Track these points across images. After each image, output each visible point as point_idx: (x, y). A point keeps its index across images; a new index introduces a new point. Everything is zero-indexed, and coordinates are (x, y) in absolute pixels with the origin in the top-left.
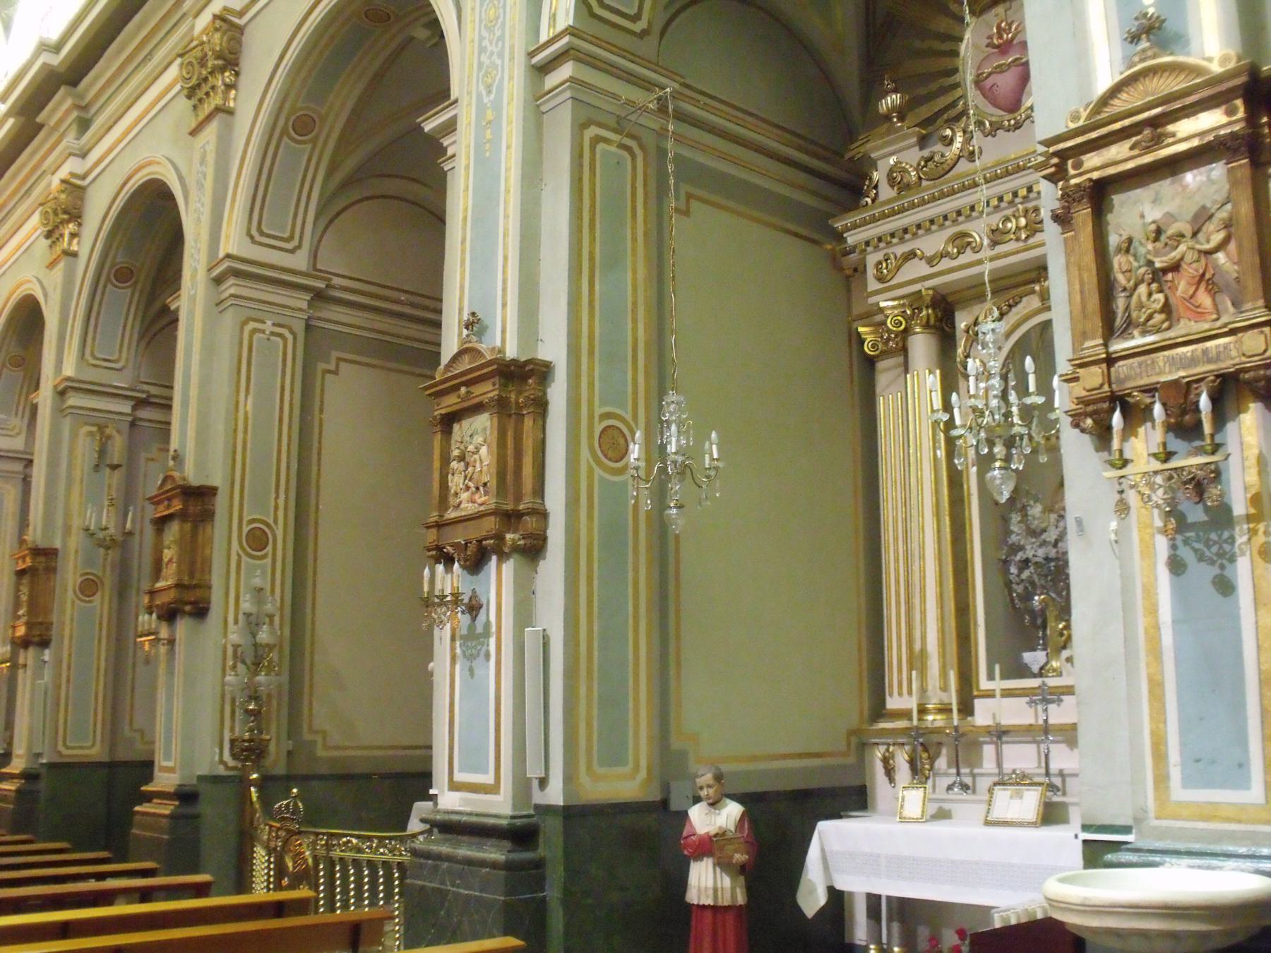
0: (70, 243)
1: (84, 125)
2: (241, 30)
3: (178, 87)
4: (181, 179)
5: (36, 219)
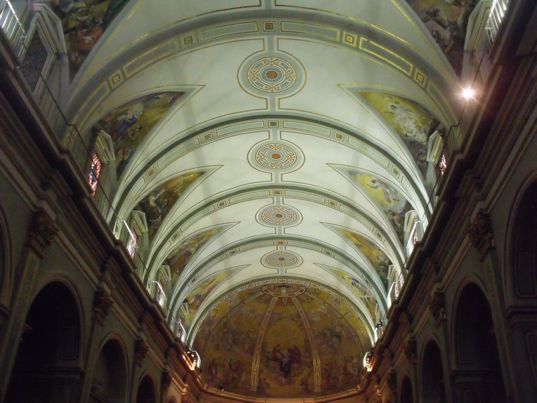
0: (443, 316)
1: (437, 269)
2: (488, 215)
3: (470, 244)
4: (482, 281)
5: (428, 309)
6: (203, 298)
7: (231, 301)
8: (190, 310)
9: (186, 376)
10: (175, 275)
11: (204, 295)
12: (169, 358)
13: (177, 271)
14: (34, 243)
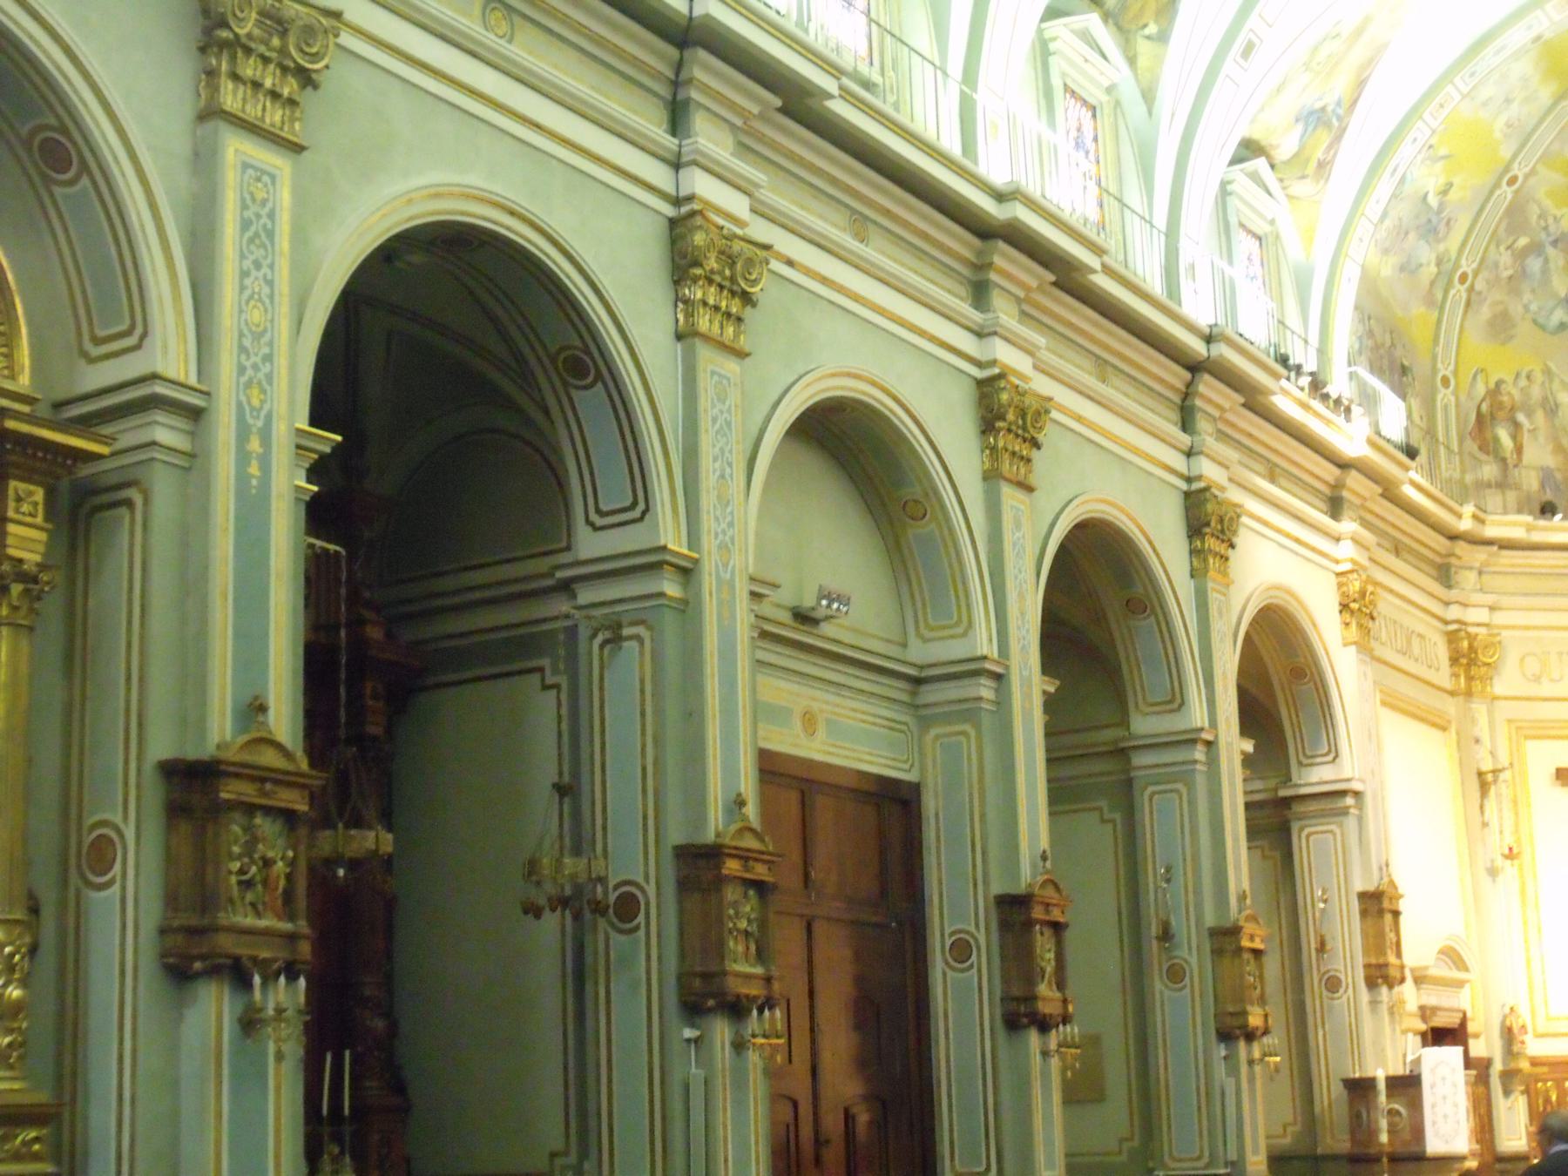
6: (1339, 118)
7: (1508, 101)
8: (1291, 191)
9: (1337, 486)
10: (1143, 48)
11: (1339, 104)
12: (1203, 424)
13: (1145, 26)
14: (231, 98)
